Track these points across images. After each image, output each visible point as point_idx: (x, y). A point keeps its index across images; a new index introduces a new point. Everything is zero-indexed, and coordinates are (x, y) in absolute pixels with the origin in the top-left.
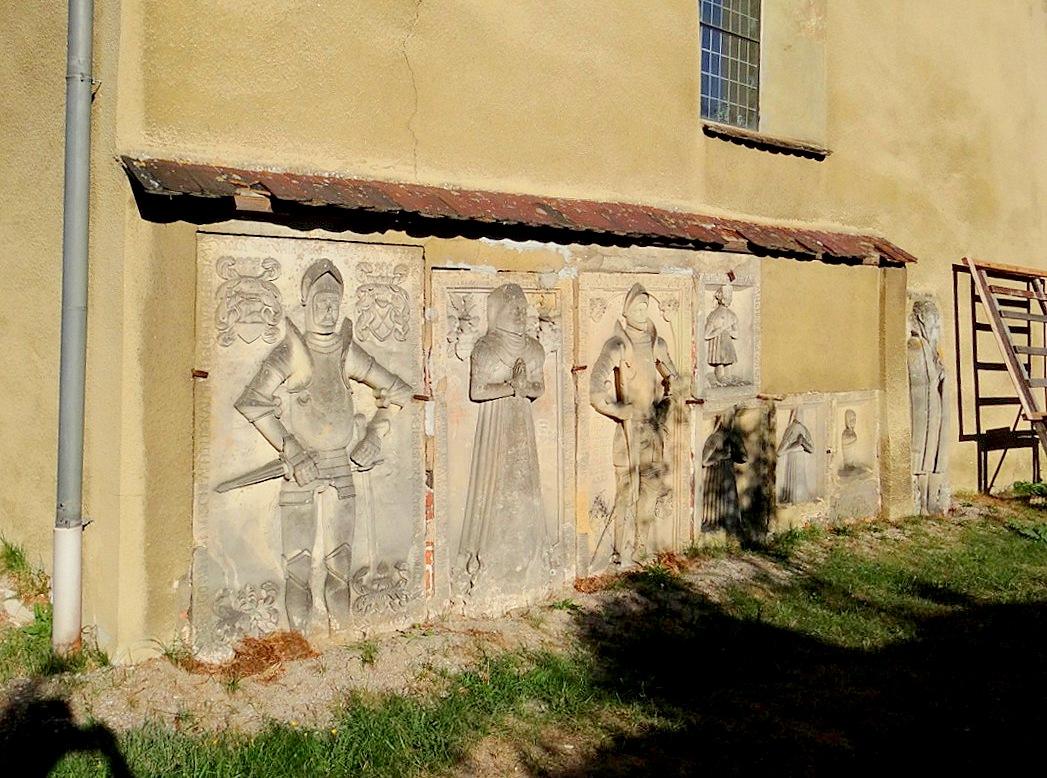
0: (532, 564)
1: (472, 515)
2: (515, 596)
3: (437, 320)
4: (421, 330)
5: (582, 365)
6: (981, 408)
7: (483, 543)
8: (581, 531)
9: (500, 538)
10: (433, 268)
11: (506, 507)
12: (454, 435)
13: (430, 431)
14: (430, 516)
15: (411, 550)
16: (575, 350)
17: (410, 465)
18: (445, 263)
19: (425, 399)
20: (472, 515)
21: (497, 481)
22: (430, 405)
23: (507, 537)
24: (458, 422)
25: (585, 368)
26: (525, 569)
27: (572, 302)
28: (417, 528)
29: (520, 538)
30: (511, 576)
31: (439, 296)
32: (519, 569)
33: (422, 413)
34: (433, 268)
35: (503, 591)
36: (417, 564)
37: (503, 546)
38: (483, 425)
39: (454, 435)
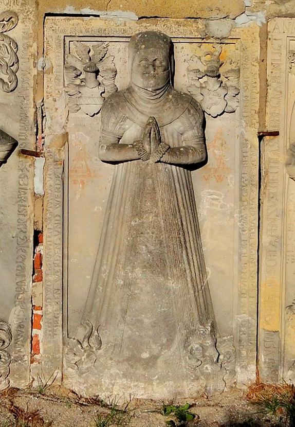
0: (166, 354)
1: (97, 285)
2: (142, 385)
3: (51, 70)
4: (32, 81)
5: (270, 129)
6: (47, 17)
7: (103, 319)
8: (268, 328)
9: (119, 317)
10: (47, 15)
11: (128, 284)
12: (78, 197)
13: (39, 189)
14: (39, 279)
15: (13, 310)
16: (262, 112)
17: (15, 221)
18: (64, 8)
19: (36, 154)
20: (97, 285)
21: (119, 254)
22: (40, 162)
23: (128, 318)
24: (82, 182)
25: (276, 134)
26: (154, 358)
27: (258, 54)
28: (20, 288)
29: (146, 321)
30: (135, 361)
31: (54, 46)
32: (145, 355)
33: (31, 169)
34: (47, 15)
35: (125, 376)
36: (20, 326)
37: (122, 327)
38: (114, 188)
39: (78, 197)
